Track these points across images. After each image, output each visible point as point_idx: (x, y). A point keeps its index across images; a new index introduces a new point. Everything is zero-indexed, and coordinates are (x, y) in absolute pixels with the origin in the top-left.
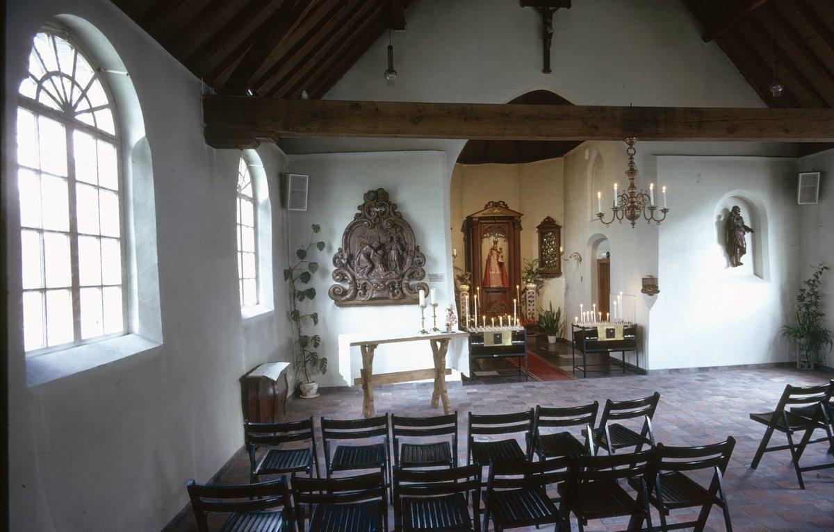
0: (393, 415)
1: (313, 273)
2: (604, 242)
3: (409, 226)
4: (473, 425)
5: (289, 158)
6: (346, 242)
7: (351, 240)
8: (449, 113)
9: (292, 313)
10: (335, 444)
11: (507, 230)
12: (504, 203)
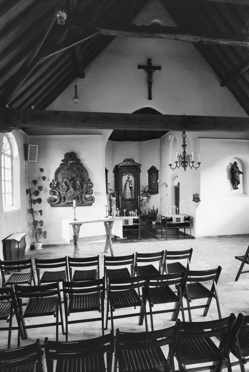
0: (69, 257)
1: (40, 191)
2: (178, 177)
3: (86, 170)
4: (106, 262)
5: (29, 137)
6: (56, 177)
7: (59, 176)
8: (100, 117)
9: (30, 210)
10: (42, 271)
11: (134, 172)
12: (132, 159)
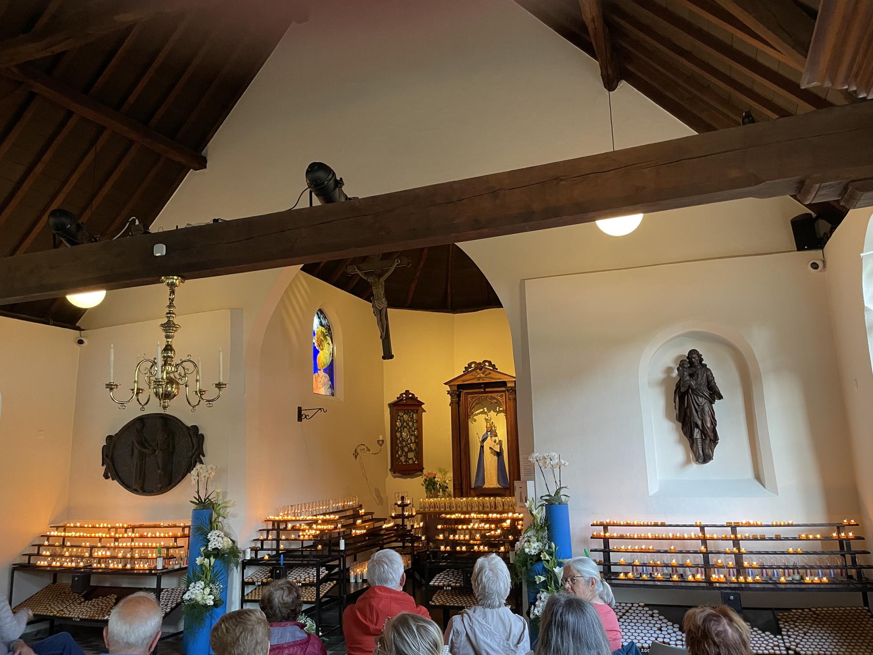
12: (490, 362)
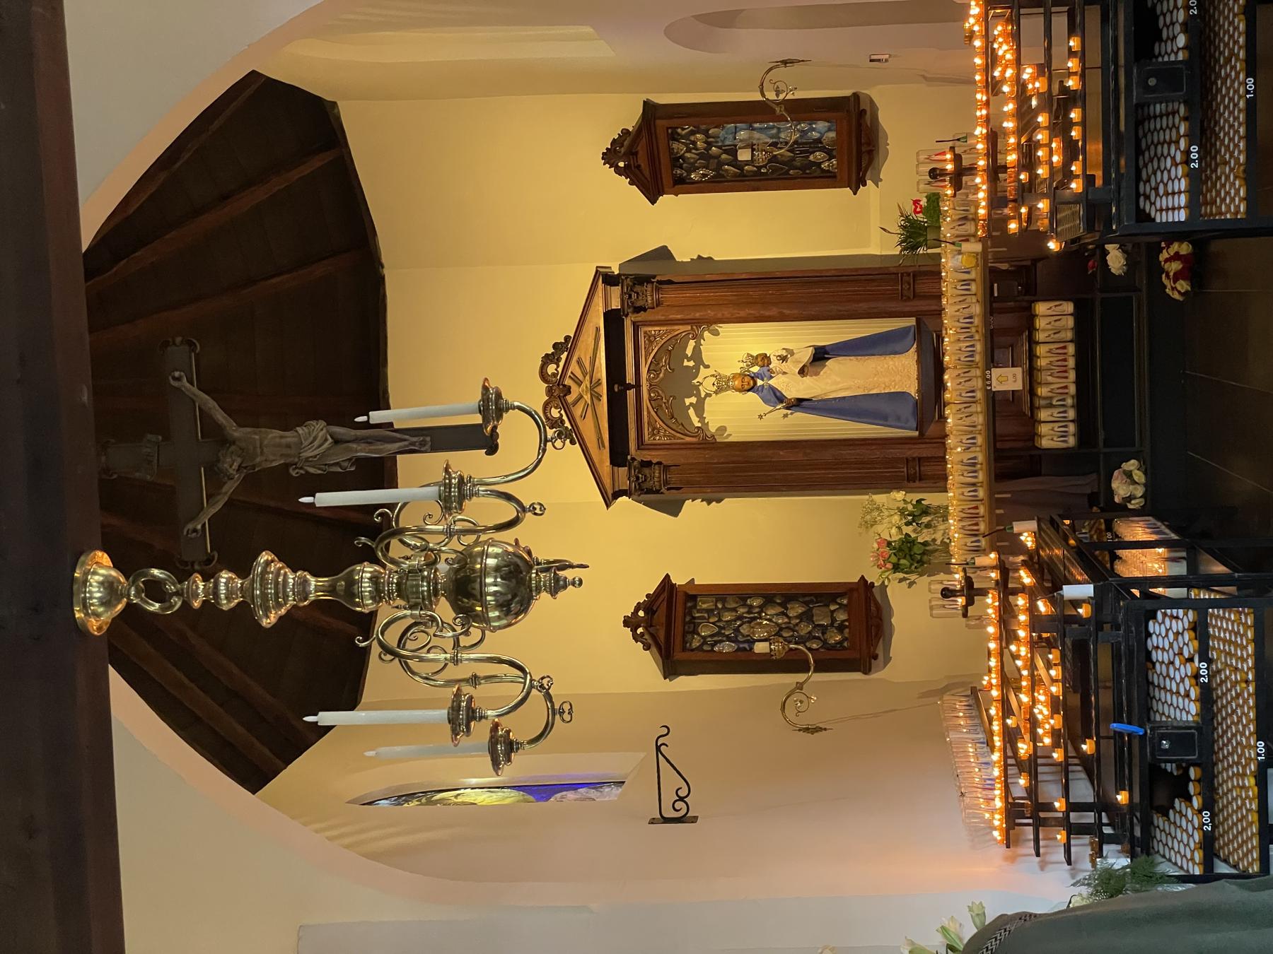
12: (547, 359)
